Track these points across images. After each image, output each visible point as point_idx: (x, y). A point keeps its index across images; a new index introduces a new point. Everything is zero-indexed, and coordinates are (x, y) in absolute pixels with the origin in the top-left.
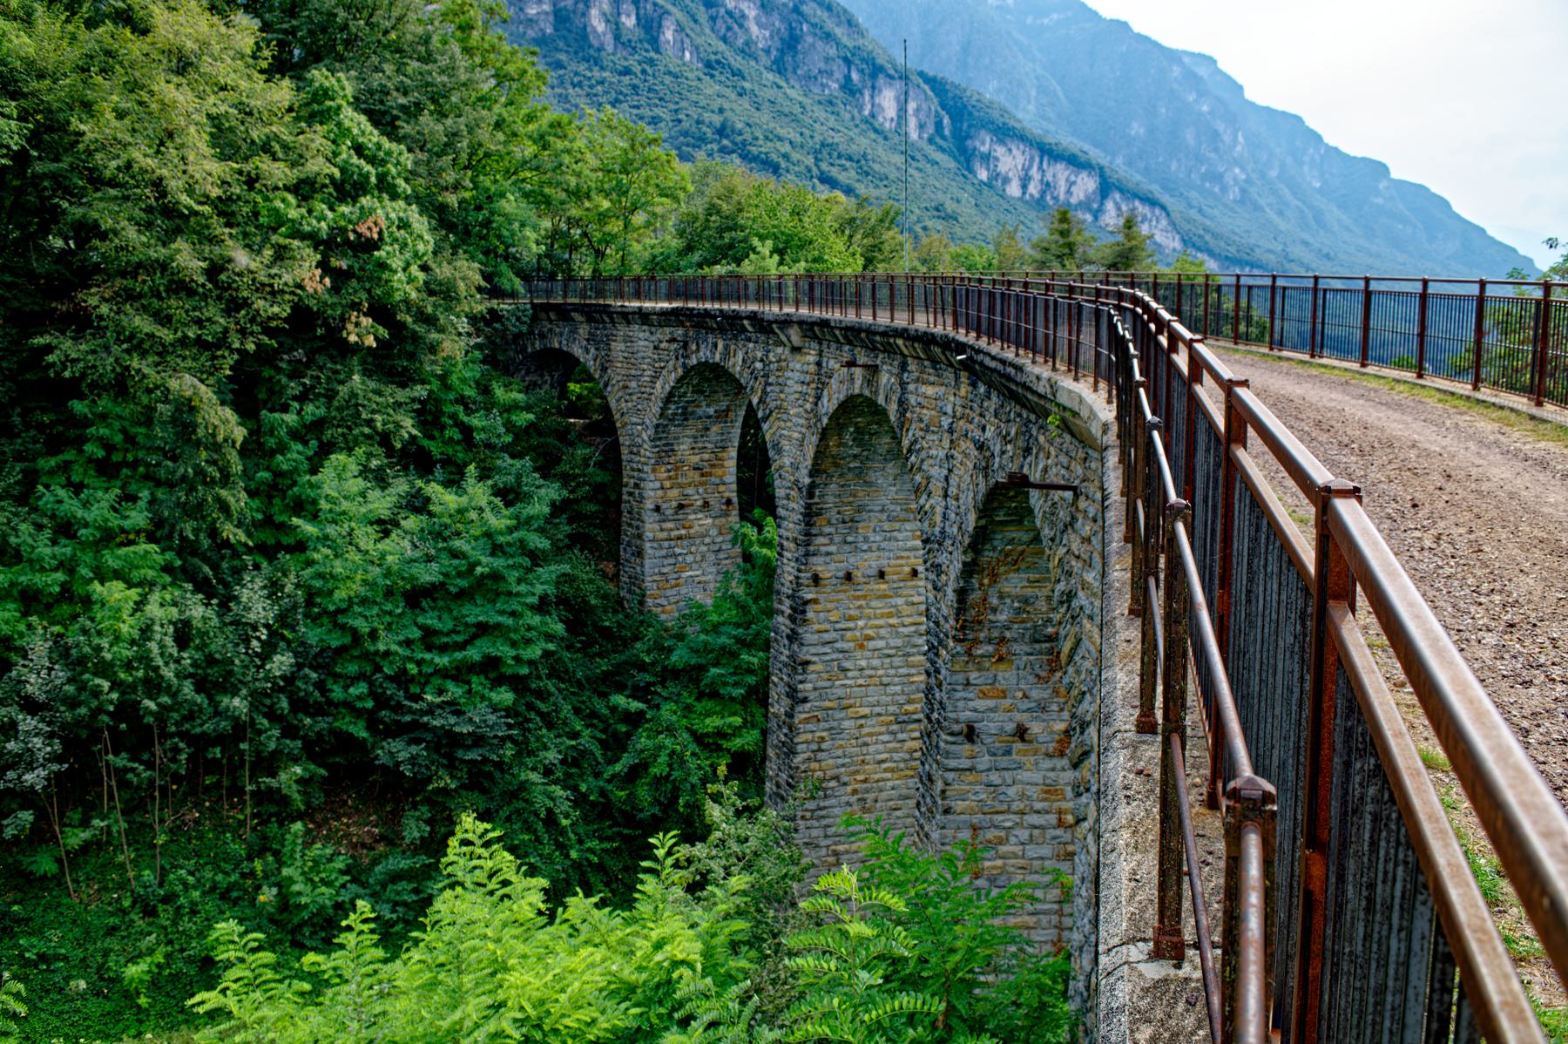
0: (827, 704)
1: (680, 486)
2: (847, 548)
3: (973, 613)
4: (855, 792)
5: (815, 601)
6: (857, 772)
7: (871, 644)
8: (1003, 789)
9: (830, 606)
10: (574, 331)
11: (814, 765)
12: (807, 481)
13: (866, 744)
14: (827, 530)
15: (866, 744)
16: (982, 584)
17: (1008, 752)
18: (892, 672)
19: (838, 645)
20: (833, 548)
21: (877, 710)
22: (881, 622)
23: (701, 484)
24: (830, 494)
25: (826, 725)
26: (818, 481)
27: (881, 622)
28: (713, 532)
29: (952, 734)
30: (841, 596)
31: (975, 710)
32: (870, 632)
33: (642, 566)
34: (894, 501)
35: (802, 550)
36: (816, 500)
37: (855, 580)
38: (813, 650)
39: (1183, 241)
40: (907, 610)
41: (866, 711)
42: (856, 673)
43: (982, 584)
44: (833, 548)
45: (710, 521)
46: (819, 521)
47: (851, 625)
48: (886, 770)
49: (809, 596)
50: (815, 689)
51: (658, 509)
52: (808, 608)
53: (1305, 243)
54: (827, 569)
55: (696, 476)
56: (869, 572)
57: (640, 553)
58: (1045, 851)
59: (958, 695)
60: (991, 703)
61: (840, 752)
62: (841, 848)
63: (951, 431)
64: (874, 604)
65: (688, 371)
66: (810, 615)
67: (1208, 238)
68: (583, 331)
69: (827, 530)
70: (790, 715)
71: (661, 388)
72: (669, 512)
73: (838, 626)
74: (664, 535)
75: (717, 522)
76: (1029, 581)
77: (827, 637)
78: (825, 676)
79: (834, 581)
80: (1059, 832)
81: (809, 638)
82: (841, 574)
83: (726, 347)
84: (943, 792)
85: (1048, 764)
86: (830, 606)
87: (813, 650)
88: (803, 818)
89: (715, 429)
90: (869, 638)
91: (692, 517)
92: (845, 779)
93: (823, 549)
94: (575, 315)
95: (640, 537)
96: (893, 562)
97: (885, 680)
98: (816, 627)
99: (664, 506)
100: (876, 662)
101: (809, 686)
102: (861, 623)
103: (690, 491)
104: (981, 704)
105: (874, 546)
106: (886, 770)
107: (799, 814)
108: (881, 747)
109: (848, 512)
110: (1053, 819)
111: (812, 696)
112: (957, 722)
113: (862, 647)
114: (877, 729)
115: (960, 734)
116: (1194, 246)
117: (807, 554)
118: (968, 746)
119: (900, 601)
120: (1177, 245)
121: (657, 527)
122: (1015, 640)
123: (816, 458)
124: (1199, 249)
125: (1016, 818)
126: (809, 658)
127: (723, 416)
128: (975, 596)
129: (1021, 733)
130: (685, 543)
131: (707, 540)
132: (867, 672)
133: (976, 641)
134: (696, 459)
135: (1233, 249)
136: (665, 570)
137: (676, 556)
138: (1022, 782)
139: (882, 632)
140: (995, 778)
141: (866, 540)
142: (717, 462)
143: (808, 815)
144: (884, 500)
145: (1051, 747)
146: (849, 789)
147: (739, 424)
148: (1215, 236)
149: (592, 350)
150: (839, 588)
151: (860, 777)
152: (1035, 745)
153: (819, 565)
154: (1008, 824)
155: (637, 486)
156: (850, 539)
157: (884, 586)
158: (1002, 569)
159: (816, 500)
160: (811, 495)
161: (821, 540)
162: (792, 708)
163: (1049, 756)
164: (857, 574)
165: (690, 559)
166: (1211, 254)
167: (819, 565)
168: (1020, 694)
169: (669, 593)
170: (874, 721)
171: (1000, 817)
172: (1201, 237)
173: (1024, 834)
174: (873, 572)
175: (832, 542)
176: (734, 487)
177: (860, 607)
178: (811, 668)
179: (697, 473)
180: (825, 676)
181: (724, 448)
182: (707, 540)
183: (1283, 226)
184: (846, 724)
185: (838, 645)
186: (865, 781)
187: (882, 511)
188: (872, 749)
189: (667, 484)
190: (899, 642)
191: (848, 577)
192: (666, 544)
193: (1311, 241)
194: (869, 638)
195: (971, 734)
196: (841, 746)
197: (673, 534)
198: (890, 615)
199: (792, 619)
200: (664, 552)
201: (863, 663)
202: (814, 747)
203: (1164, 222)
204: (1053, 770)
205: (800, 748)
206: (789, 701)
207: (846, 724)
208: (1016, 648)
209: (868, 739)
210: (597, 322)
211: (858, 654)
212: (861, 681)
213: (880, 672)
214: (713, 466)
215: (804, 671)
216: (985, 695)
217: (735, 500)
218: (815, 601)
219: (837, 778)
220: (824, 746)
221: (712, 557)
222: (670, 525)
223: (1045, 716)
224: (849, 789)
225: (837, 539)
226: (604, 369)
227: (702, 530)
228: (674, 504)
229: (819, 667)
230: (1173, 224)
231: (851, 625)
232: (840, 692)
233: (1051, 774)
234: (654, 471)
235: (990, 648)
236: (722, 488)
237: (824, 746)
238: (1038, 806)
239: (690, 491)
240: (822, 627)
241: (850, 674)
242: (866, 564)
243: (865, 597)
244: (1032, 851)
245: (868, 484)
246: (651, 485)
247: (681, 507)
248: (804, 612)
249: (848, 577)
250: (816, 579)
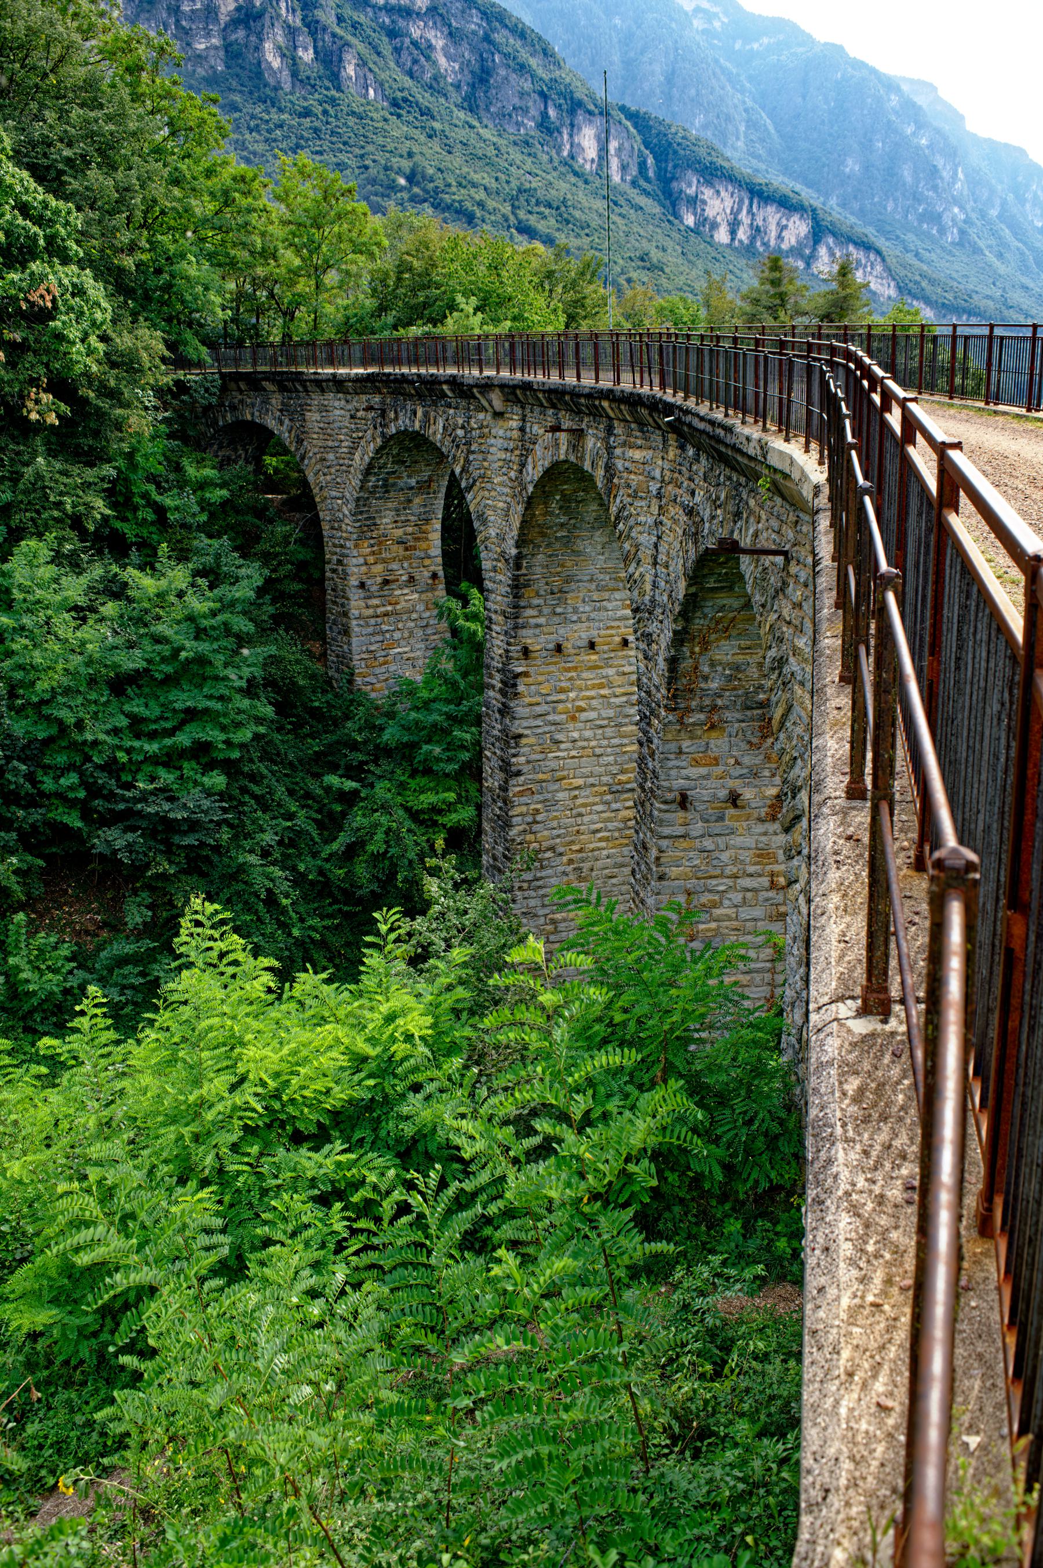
0: (541, 776)
1: (384, 561)
2: (556, 619)
3: (684, 681)
4: (571, 861)
5: (526, 674)
6: (572, 842)
7: (584, 716)
8: (716, 854)
9: (541, 678)
10: (266, 402)
11: (530, 837)
12: (514, 551)
13: (580, 815)
14: (536, 601)
15: (580, 815)
16: (693, 653)
17: (721, 819)
18: (605, 743)
19: (550, 718)
20: (542, 620)
21: (591, 780)
22: (592, 693)
23: (406, 558)
24: (538, 564)
25: (541, 798)
26: (525, 551)
27: (592, 693)
28: (420, 607)
29: (665, 802)
30: (552, 668)
31: (688, 778)
32: (582, 704)
33: (349, 644)
34: (603, 570)
35: (510, 623)
36: (524, 571)
37: (565, 651)
38: (525, 724)
39: (899, 288)
40: (618, 680)
41: (580, 782)
42: (569, 745)
43: (693, 653)
44: (542, 620)
45: (416, 596)
46: (527, 592)
47: (563, 697)
48: (601, 840)
49: (520, 670)
50: (528, 762)
51: (362, 585)
52: (519, 681)
53: (1025, 288)
54: (537, 641)
55: (400, 550)
56: (579, 643)
57: (346, 632)
58: (758, 912)
59: (671, 764)
60: (703, 771)
61: (555, 824)
62: (558, 916)
63: (659, 496)
64: (585, 675)
65: (387, 440)
66: (521, 688)
67: (924, 284)
68: (276, 400)
69: (536, 601)
70: (504, 789)
71: (360, 460)
72: (374, 588)
73: (549, 699)
74: (371, 612)
75: (424, 596)
76: (740, 648)
77: (538, 710)
78: (538, 748)
79: (544, 653)
80: (771, 894)
81: (521, 711)
82: (551, 646)
83: (426, 415)
84: (658, 859)
85: (760, 828)
86: (541, 678)
87: (525, 724)
88: (520, 888)
89: (417, 500)
90: (582, 710)
91: (398, 592)
92: (561, 849)
93: (532, 621)
94: (266, 384)
95: (345, 614)
96: (603, 632)
97: (598, 751)
98: (527, 700)
99: (369, 582)
100: (588, 734)
101: (522, 759)
102: (572, 695)
103: (394, 566)
104: (694, 772)
105: (584, 617)
106: (601, 840)
107: (517, 885)
108: (595, 817)
109: (557, 582)
110: (765, 881)
111: (525, 769)
112: (670, 790)
113: (574, 718)
114: (591, 800)
115: (673, 802)
116: (910, 293)
117: (516, 627)
118: (681, 814)
119: (611, 672)
120: (892, 292)
121: (362, 604)
122: (727, 707)
123: (522, 528)
124: (915, 297)
125: (729, 882)
126: (521, 731)
127: (424, 487)
128: (686, 665)
129: (734, 799)
130: (392, 619)
131: (414, 616)
132: (580, 744)
133: (688, 710)
134: (399, 532)
135: (950, 296)
136: (372, 648)
137: (383, 633)
138: (734, 847)
139: (594, 702)
140: (708, 843)
141: (575, 611)
142: (421, 536)
143: (525, 885)
144: (592, 569)
145: (763, 812)
146: (565, 859)
147: (442, 495)
148: (932, 282)
149: (287, 422)
150: (550, 660)
151: (575, 848)
152: (748, 810)
153: (528, 638)
154: (722, 888)
155: (340, 562)
156: (559, 610)
157: (594, 657)
158: (713, 637)
159: (524, 571)
160: (518, 567)
161: (530, 612)
162: (506, 782)
163: (761, 820)
164: (568, 647)
165: (397, 635)
166: (928, 301)
167: (528, 638)
168: (732, 761)
169: (378, 671)
170: (588, 792)
171: (714, 882)
172: (916, 283)
173: (737, 897)
174: (584, 643)
175: (540, 614)
176: (439, 560)
177: (571, 679)
178: (524, 741)
179: (401, 548)
180: (538, 748)
181: (427, 521)
182: (414, 616)
183: (1002, 269)
184: (560, 795)
185: (550, 718)
186: (580, 851)
187: (591, 580)
188: (586, 819)
189: (371, 559)
190: (611, 713)
191: (559, 648)
192: (372, 621)
193: (1031, 285)
194: (582, 710)
195: (684, 802)
196: (556, 818)
197: (380, 610)
198: (601, 686)
199: (503, 693)
200: (370, 630)
201: (576, 735)
202: (529, 819)
203: (879, 268)
204: (765, 834)
205: (515, 820)
206: (502, 775)
207: (560, 795)
208: (728, 715)
209: (583, 810)
210: (290, 391)
211: (571, 726)
212: (574, 753)
213: (593, 743)
214: (417, 539)
215: (517, 745)
216: (697, 763)
217: (441, 574)
218: (526, 674)
219: (552, 849)
220: (539, 818)
221: (419, 633)
222: (375, 602)
223: (756, 782)
224: (565, 859)
225: (546, 610)
226: (300, 441)
227: (409, 605)
228: (379, 580)
229: (532, 740)
230: (888, 269)
231: (563, 697)
232: (553, 764)
233: (763, 838)
234: (356, 546)
235: (702, 717)
236: (427, 562)
237: (539, 818)
238: (751, 869)
239: (394, 566)
240: (534, 700)
241: (563, 746)
242: (576, 635)
243: (575, 669)
244: (745, 913)
245: (577, 553)
246: (354, 561)
247: (386, 582)
248: (515, 685)
249: (559, 648)
250: (526, 652)
